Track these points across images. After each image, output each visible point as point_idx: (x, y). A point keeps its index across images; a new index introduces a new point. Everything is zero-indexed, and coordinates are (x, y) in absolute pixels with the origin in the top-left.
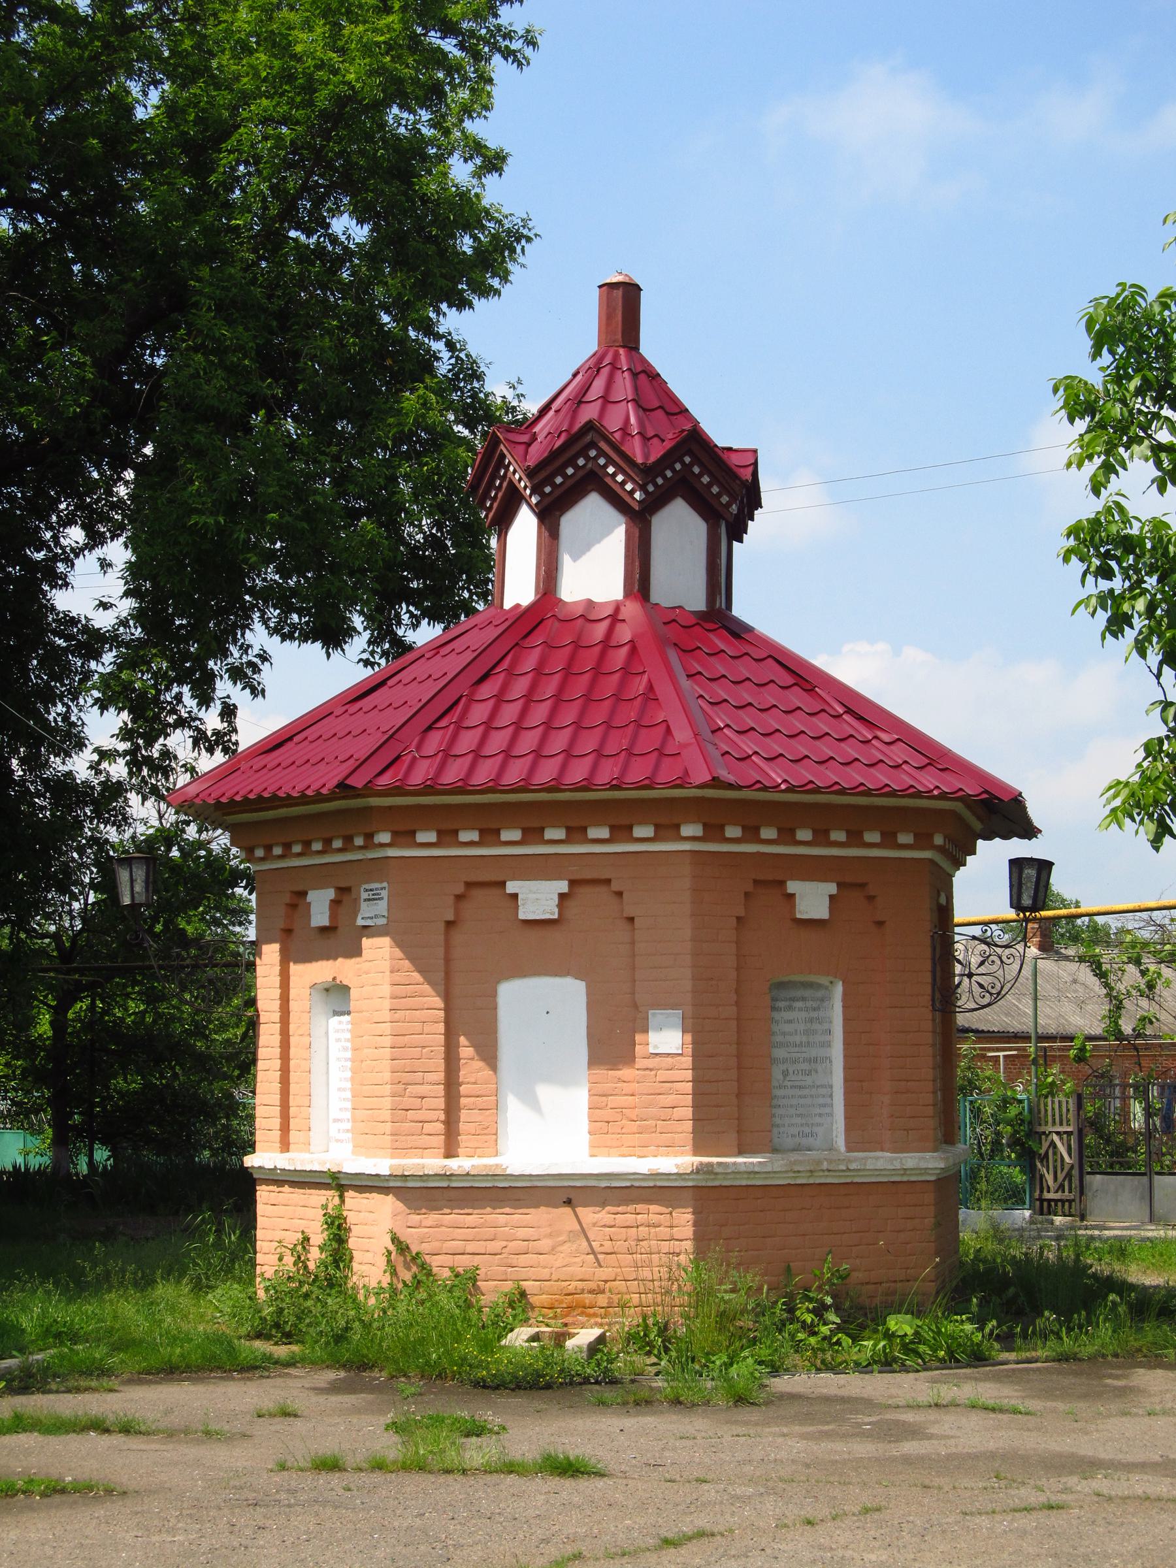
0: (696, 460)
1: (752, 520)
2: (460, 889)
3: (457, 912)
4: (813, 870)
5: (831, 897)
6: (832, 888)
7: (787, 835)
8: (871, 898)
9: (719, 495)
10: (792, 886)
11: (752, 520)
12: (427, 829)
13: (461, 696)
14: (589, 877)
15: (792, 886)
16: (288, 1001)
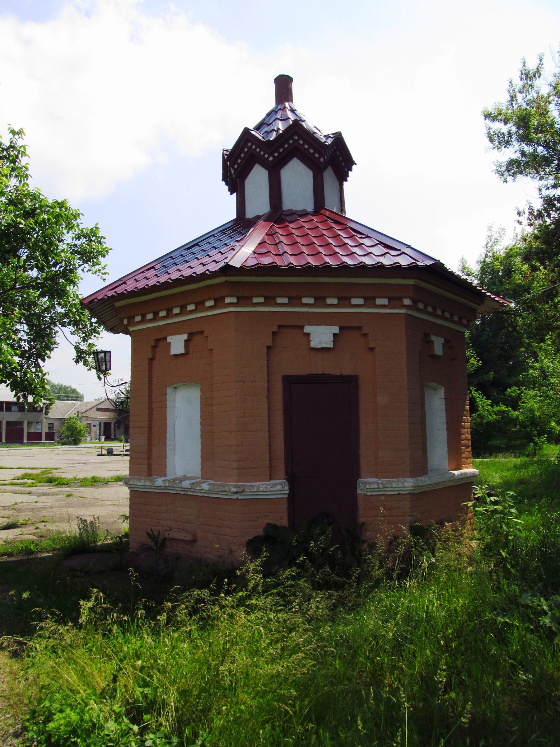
0: (301, 137)
1: (351, 170)
2: (275, 329)
3: (273, 342)
4: (176, 329)
5: (335, 335)
6: (336, 330)
7: (320, 300)
8: (365, 335)
9: (289, 144)
10: (308, 329)
11: (351, 170)
12: (332, 297)
13: (399, 250)
14: (289, 323)
15: (308, 329)
16: (152, 409)
